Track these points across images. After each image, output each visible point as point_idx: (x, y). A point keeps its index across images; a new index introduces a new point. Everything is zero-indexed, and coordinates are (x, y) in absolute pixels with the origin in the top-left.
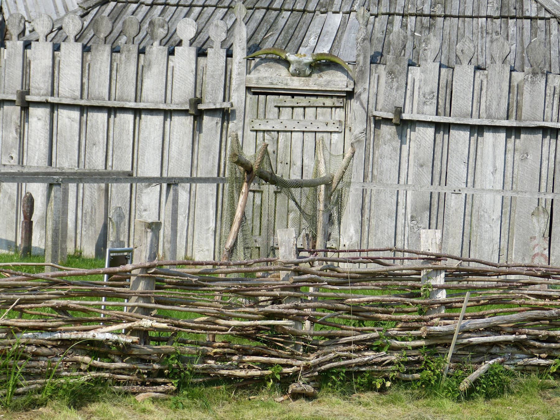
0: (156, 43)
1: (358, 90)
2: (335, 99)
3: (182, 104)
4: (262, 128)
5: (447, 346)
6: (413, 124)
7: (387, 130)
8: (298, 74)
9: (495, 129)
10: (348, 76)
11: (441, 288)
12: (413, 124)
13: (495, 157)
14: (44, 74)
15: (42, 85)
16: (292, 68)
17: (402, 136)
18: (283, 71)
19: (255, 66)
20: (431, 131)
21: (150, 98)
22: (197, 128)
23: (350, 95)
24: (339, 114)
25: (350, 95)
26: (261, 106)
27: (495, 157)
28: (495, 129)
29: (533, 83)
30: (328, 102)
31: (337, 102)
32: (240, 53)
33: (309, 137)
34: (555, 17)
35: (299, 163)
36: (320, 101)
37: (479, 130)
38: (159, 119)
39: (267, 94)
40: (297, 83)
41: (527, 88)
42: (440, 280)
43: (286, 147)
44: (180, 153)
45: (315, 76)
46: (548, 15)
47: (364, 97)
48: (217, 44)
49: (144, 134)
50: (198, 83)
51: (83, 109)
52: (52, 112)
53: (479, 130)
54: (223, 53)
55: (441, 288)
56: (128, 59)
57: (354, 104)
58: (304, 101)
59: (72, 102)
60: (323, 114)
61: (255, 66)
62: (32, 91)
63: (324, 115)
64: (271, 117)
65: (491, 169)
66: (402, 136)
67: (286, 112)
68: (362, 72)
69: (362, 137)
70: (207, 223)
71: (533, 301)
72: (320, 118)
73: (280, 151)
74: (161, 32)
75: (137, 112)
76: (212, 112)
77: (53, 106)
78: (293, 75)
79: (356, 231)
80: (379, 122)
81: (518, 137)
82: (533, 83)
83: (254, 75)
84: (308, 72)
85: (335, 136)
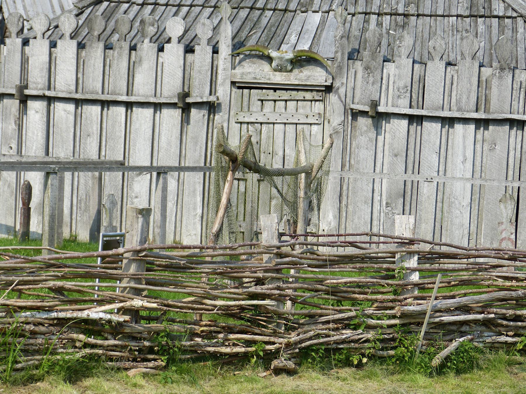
0: (147, 41)
1: (337, 84)
2: (315, 93)
3: (171, 97)
4: (247, 120)
5: (420, 324)
6: (388, 116)
7: (364, 122)
8: (280, 69)
9: (465, 121)
10: (327, 71)
11: (414, 270)
12: (388, 116)
13: (464, 147)
14: (42, 70)
15: (39, 80)
16: (274, 64)
17: (377, 127)
18: (266, 67)
19: (240, 62)
20: (404, 123)
21: (141, 92)
22: (185, 120)
23: (329, 89)
24: (318, 107)
25: (329, 89)
26: (246, 99)
27: (464, 147)
28: (465, 121)
29: (500, 77)
30: (308, 96)
31: (317, 96)
32: (225, 50)
33: (291, 129)
34: (521, 16)
35: (281, 153)
36: (301, 95)
37: (450, 122)
38: (149, 112)
39: (250, 88)
40: (279, 78)
41: (495, 82)
42: (413, 262)
43: (269, 137)
44: (169, 143)
45: (296, 71)
46: (515, 14)
47: (342, 91)
48: (204, 42)
49: (135, 126)
50: (186, 78)
51: (78, 102)
52: (49, 105)
53: (450, 122)
54: (210, 49)
55: (414, 270)
56: (120, 55)
57: (332, 97)
58: (285, 95)
59: (67, 96)
60: (304, 107)
61: (240, 62)
62: (31, 85)
63: (305, 108)
64: (255, 110)
65: (461, 158)
66: (377, 127)
67: (269, 106)
68: (340, 68)
69: (340, 129)
70: (195, 209)
71: (500, 282)
72: (301, 111)
73: (263, 142)
74: (151, 30)
75: (129, 105)
76: (199, 105)
77: (50, 100)
78: (275, 70)
79: (335, 217)
80: (356, 114)
81: (486, 128)
82: (500, 77)
83: (238, 71)
84: (289, 67)
85: (315, 128)
